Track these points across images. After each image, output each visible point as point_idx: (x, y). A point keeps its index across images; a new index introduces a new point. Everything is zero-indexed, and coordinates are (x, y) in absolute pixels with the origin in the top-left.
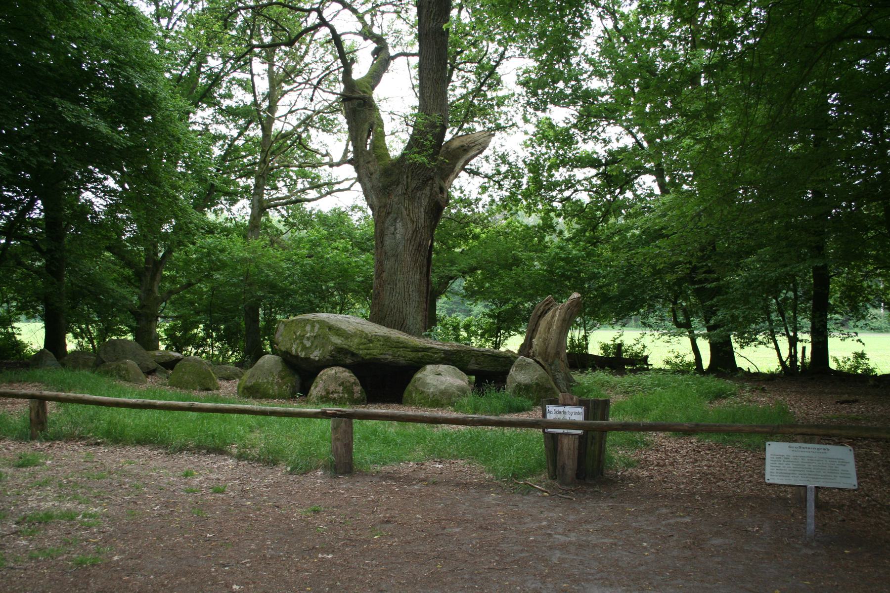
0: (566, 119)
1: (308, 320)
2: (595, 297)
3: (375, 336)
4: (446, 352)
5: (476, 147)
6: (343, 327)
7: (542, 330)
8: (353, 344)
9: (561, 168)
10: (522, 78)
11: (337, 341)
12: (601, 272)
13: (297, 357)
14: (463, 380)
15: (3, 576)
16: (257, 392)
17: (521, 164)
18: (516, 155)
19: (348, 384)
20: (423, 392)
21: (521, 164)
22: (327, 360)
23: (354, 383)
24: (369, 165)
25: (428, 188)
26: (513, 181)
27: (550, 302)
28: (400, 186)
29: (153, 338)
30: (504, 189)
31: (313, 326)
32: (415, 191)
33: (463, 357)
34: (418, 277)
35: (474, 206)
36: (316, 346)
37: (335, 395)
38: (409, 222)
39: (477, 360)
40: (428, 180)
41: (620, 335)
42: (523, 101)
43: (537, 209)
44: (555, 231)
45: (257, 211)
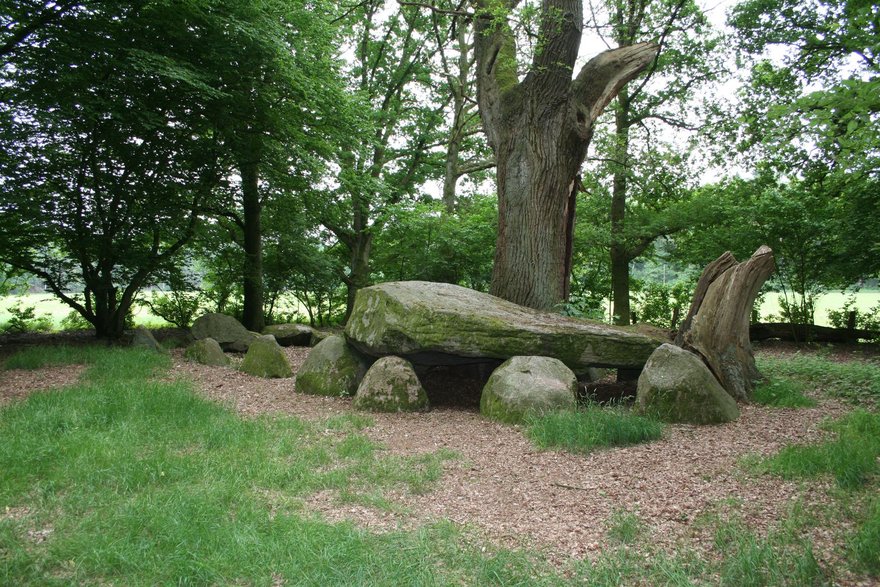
0: (786, 57)
1: (371, 290)
4: (544, 337)
5: (634, 63)
7: (708, 301)
8: (408, 326)
10: (732, 19)
11: (392, 319)
12: (824, 225)
13: (355, 340)
14: (564, 381)
16: (308, 385)
17: (733, 113)
18: (727, 103)
19: (401, 382)
21: (733, 113)
22: (380, 346)
24: (490, 94)
25: (560, 115)
26: (727, 134)
27: (729, 261)
28: (524, 114)
33: (573, 343)
34: (551, 232)
36: (373, 327)
37: (382, 398)
38: (536, 161)
39: (594, 349)
40: (559, 104)
42: (734, 43)
44: (776, 185)
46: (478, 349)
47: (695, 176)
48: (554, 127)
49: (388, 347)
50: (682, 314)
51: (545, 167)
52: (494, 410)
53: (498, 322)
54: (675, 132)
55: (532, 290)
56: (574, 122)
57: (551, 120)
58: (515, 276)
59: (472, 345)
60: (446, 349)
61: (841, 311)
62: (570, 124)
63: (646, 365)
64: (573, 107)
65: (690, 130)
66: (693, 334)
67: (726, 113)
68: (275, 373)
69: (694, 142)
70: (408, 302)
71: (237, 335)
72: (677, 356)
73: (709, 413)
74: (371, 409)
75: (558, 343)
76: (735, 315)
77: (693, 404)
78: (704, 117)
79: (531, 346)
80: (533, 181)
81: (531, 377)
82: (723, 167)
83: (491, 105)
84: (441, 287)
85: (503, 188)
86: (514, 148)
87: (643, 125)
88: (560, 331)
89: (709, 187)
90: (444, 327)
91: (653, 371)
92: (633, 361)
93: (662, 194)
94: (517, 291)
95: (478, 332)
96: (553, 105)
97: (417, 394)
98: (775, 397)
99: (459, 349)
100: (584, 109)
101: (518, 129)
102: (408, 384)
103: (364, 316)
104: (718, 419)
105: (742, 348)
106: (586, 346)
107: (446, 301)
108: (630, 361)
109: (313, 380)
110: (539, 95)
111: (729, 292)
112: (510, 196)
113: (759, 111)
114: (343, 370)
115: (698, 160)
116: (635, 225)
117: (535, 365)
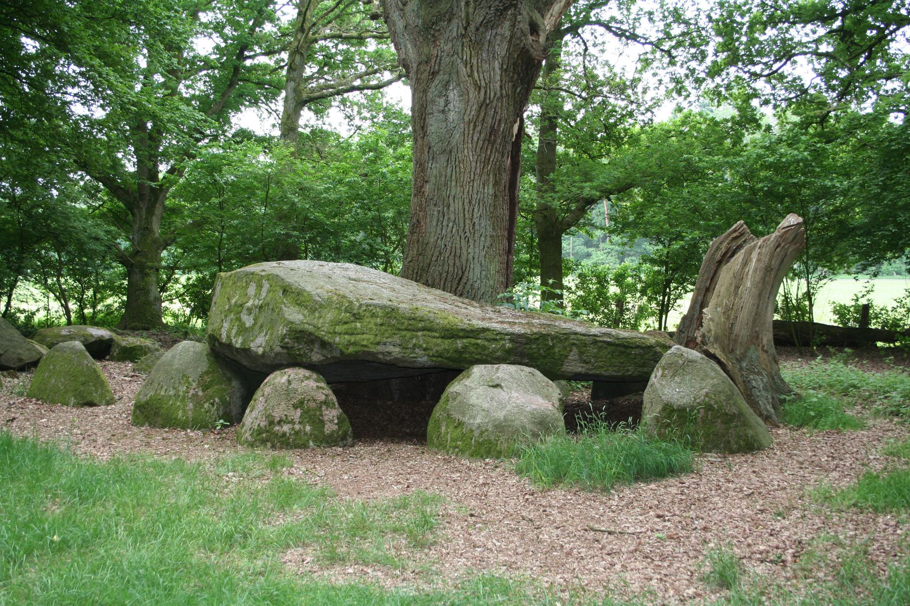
1: (253, 274)
2: (826, 229)
3: (368, 305)
4: (515, 338)
6: (309, 288)
7: (723, 289)
9: (769, 28)
11: (295, 315)
12: (838, 185)
13: (230, 346)
14: (547, 397)
16: (156, 414)
17: (703, 22)
19: (312, 405)
20: (460, 424)
21: (703, 22)
22: (277, 354)
23: (325, 403)
25: (507, 24)
26: (693, 50)
27: (742, 234)
28: (455, 21)
29: (152, 299)
30: (679, 64)
31: (260, 286)
33: (553, 347)
34: (491, 191)
35: (629, 91)
36: (261, 326)
37: (286, 428)
38: (472, 90)
39: (581, 353)
40: (506, 9)
41: (868, 292)
43: (731, 95)
44: (759, 126)
45: (292, 106)
46: (425, 355)
47: (647, 110)
48: (498, 42)
49: (289, 354)
50: (628, 310)
51: (485, 99)
52: (453, 440)
53: (451, 318)
54: (621, 47)
55: (466, 273)
56: (525, 35)
57: (494, 32)
58: (440, 253)
59: (417, 350)
60: (380, 356)
61: (849, 303)
62: (519, 38)
63: (653, 375)
64: (524, 13)
65: (643, 44)
66: (707, 334)
67: (692, 21)
68: (89, 399)
69: (646, 63)
70: (319, 291)
71: (7, 343)
72: (696, 362)
73: (739, 437)
74: (269, 444)
75: (534, 346)
76: (757, 308)
77: (719, 426)
78: (661, 25)
79: (498, 350)
80: (466, 119)
81: (503, 393)
82: (685, 99)
83: (404, 5)
84: (346, 269)
85: (423, 128)
86: (439, 70)
87: (579, 35)
88: (535, 330)
89: (666, 128)
90: (376, 325)
91: (664, 383)
92: (631, 370)
93: (599, 136)
94: (444, 275)
95: (425, 332)
96: (497, 10)
97: (336, 421)
98: (814, 417)
99: (399, 356)
100: (536, 16)
101: (446, 43)
102: (324, 408)
103: (245, 311)
104: (750, 446)
105: (766, 352)
106: (571, 351)
107: (365, 288)
108: (628, 370)
109: (165, 406)
111: (749, 277)
112: (433, 139)
113: (738, 19)
114: (210, 391)
115: (652, 87)
116: (574, 182)
117: (507, 377)
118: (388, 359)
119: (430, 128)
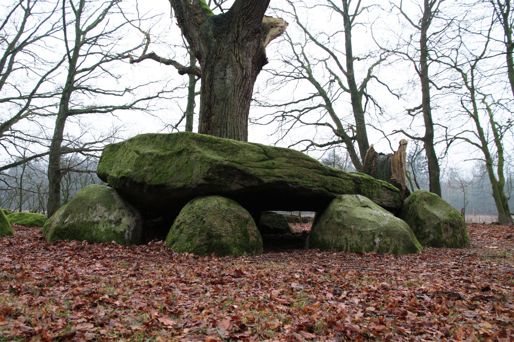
15: (511, 285)
28: (231, 34)
32: (245, 40)
38: (239, 69)
60: (290, 185)
80: (236, 84)
110: (244, 22)
118: (295, 187)
119: (215, 86)
